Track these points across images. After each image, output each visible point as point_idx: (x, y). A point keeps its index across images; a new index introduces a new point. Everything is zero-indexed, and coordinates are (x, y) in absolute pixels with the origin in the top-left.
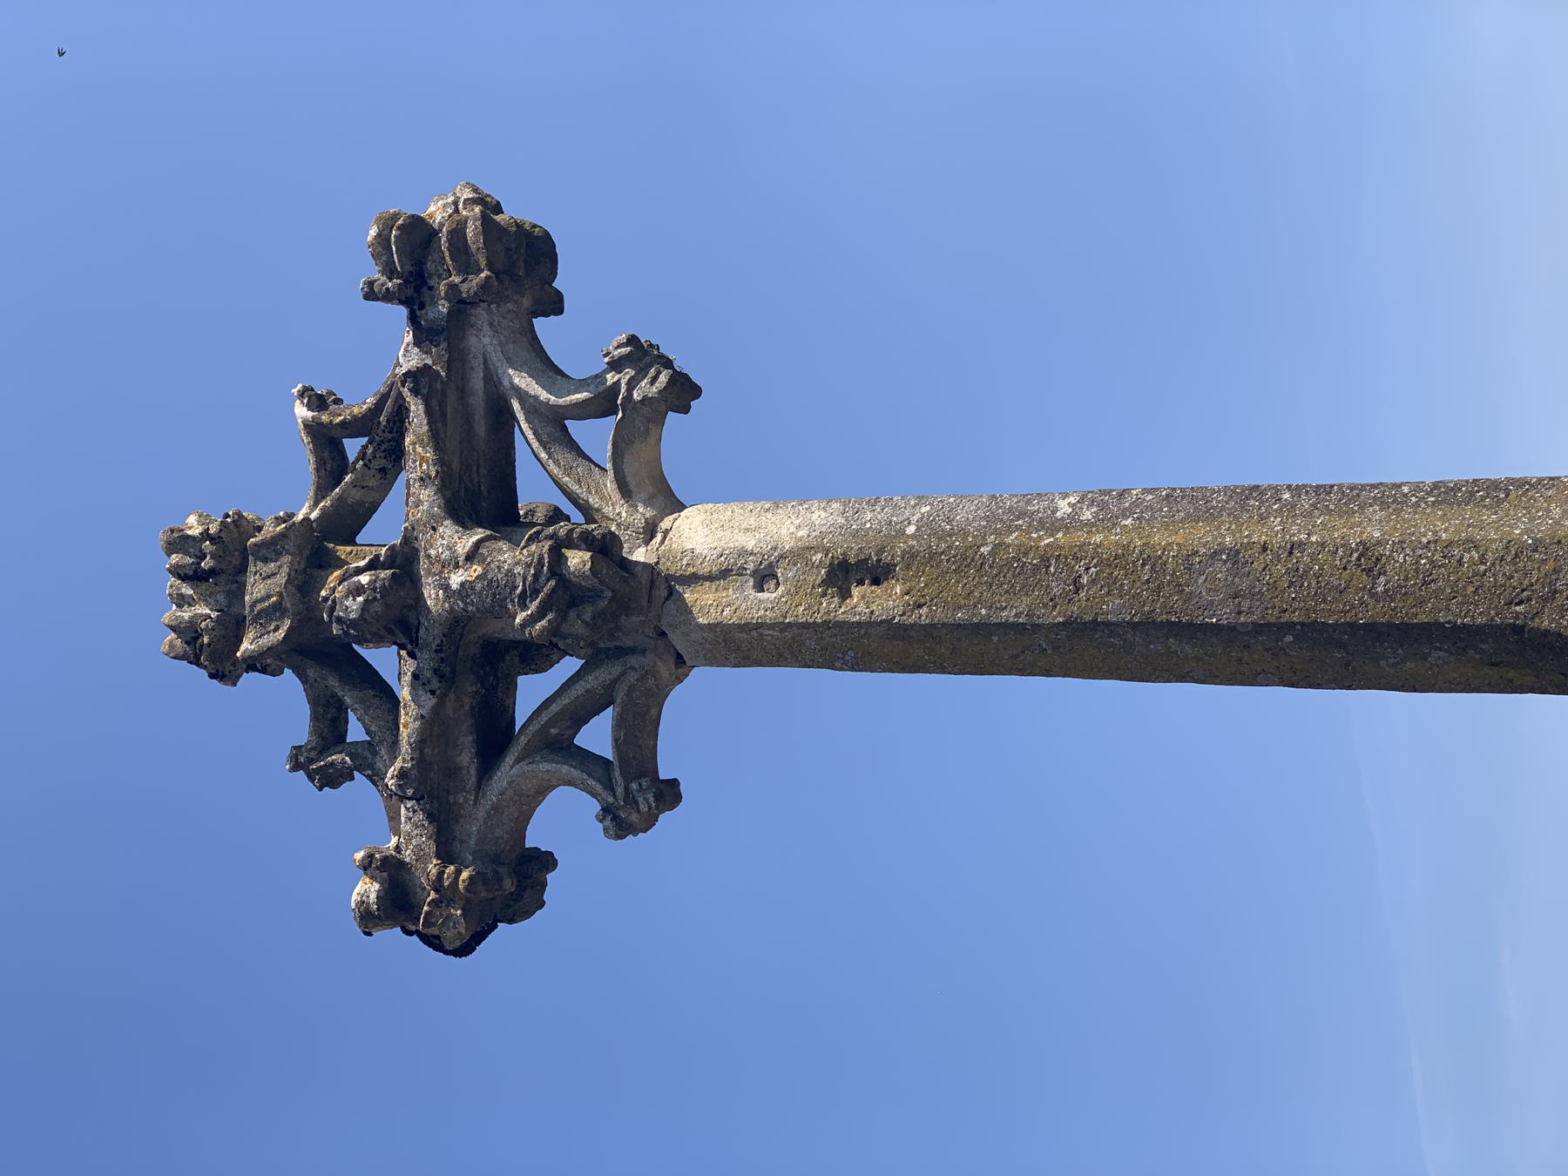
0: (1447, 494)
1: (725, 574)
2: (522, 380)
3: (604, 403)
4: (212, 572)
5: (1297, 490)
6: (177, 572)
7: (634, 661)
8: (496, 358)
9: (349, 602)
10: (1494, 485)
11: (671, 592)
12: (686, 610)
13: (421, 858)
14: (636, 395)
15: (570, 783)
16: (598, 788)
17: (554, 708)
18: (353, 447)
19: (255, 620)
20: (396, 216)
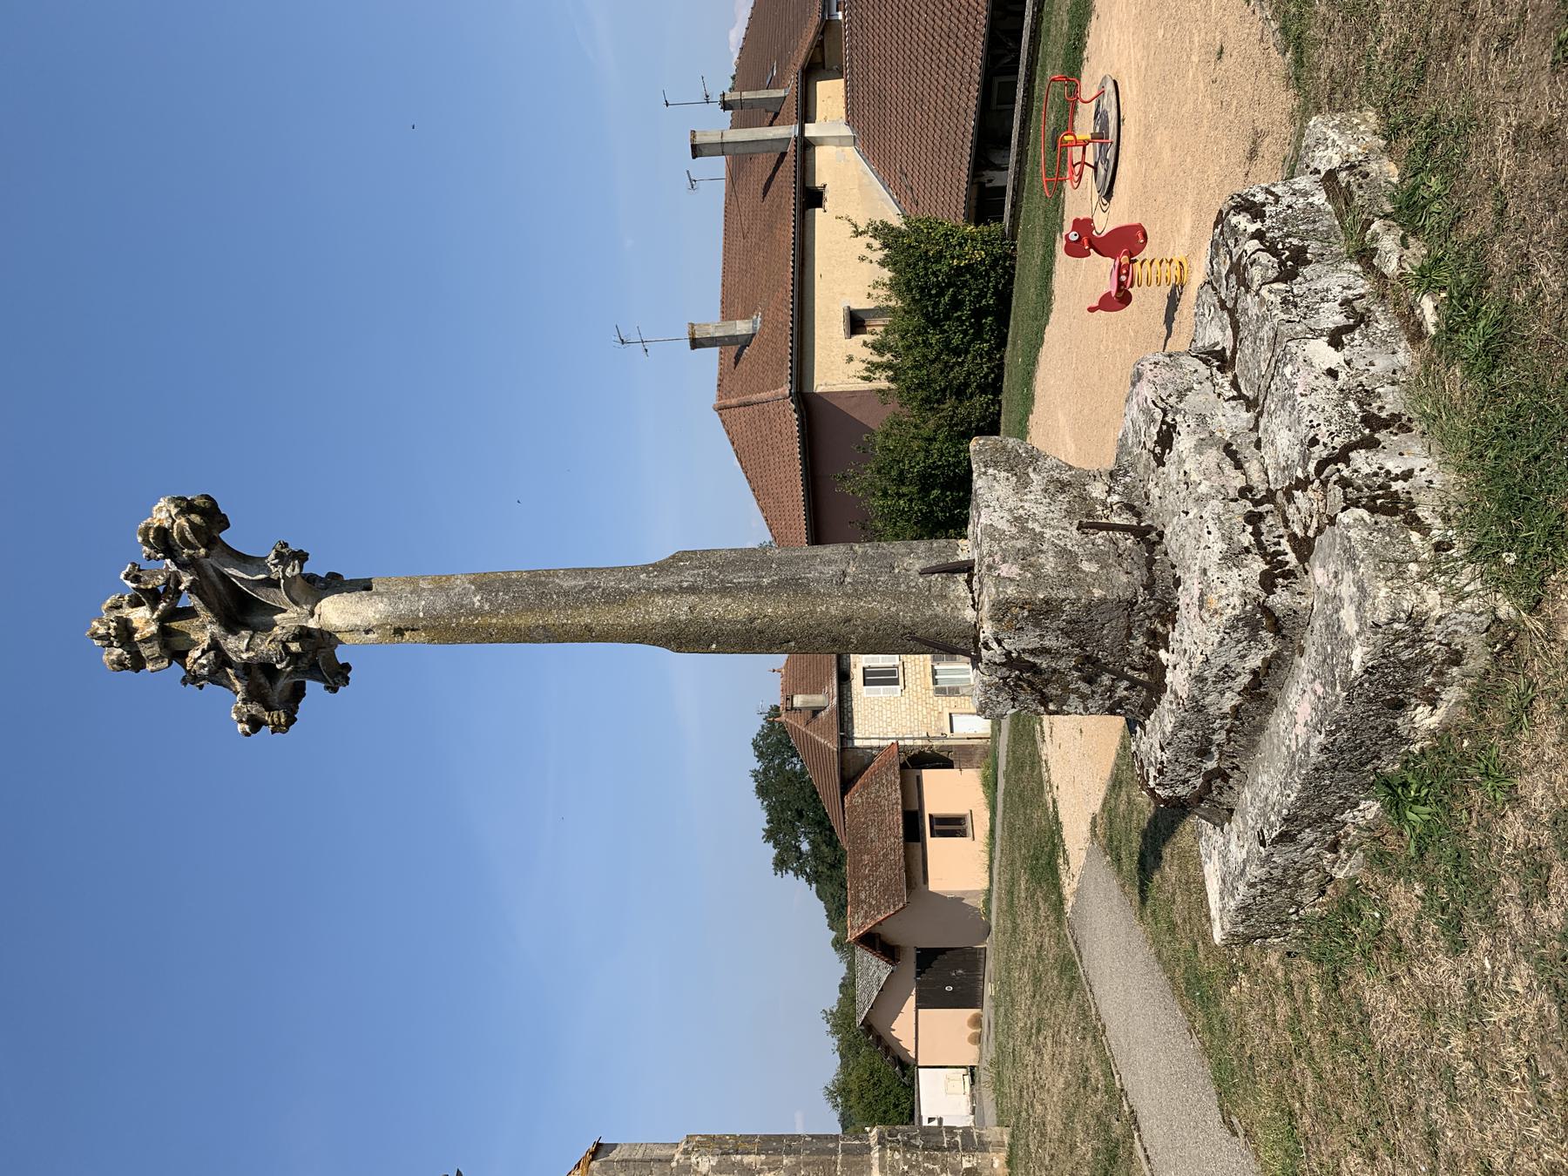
8: (217, 565)
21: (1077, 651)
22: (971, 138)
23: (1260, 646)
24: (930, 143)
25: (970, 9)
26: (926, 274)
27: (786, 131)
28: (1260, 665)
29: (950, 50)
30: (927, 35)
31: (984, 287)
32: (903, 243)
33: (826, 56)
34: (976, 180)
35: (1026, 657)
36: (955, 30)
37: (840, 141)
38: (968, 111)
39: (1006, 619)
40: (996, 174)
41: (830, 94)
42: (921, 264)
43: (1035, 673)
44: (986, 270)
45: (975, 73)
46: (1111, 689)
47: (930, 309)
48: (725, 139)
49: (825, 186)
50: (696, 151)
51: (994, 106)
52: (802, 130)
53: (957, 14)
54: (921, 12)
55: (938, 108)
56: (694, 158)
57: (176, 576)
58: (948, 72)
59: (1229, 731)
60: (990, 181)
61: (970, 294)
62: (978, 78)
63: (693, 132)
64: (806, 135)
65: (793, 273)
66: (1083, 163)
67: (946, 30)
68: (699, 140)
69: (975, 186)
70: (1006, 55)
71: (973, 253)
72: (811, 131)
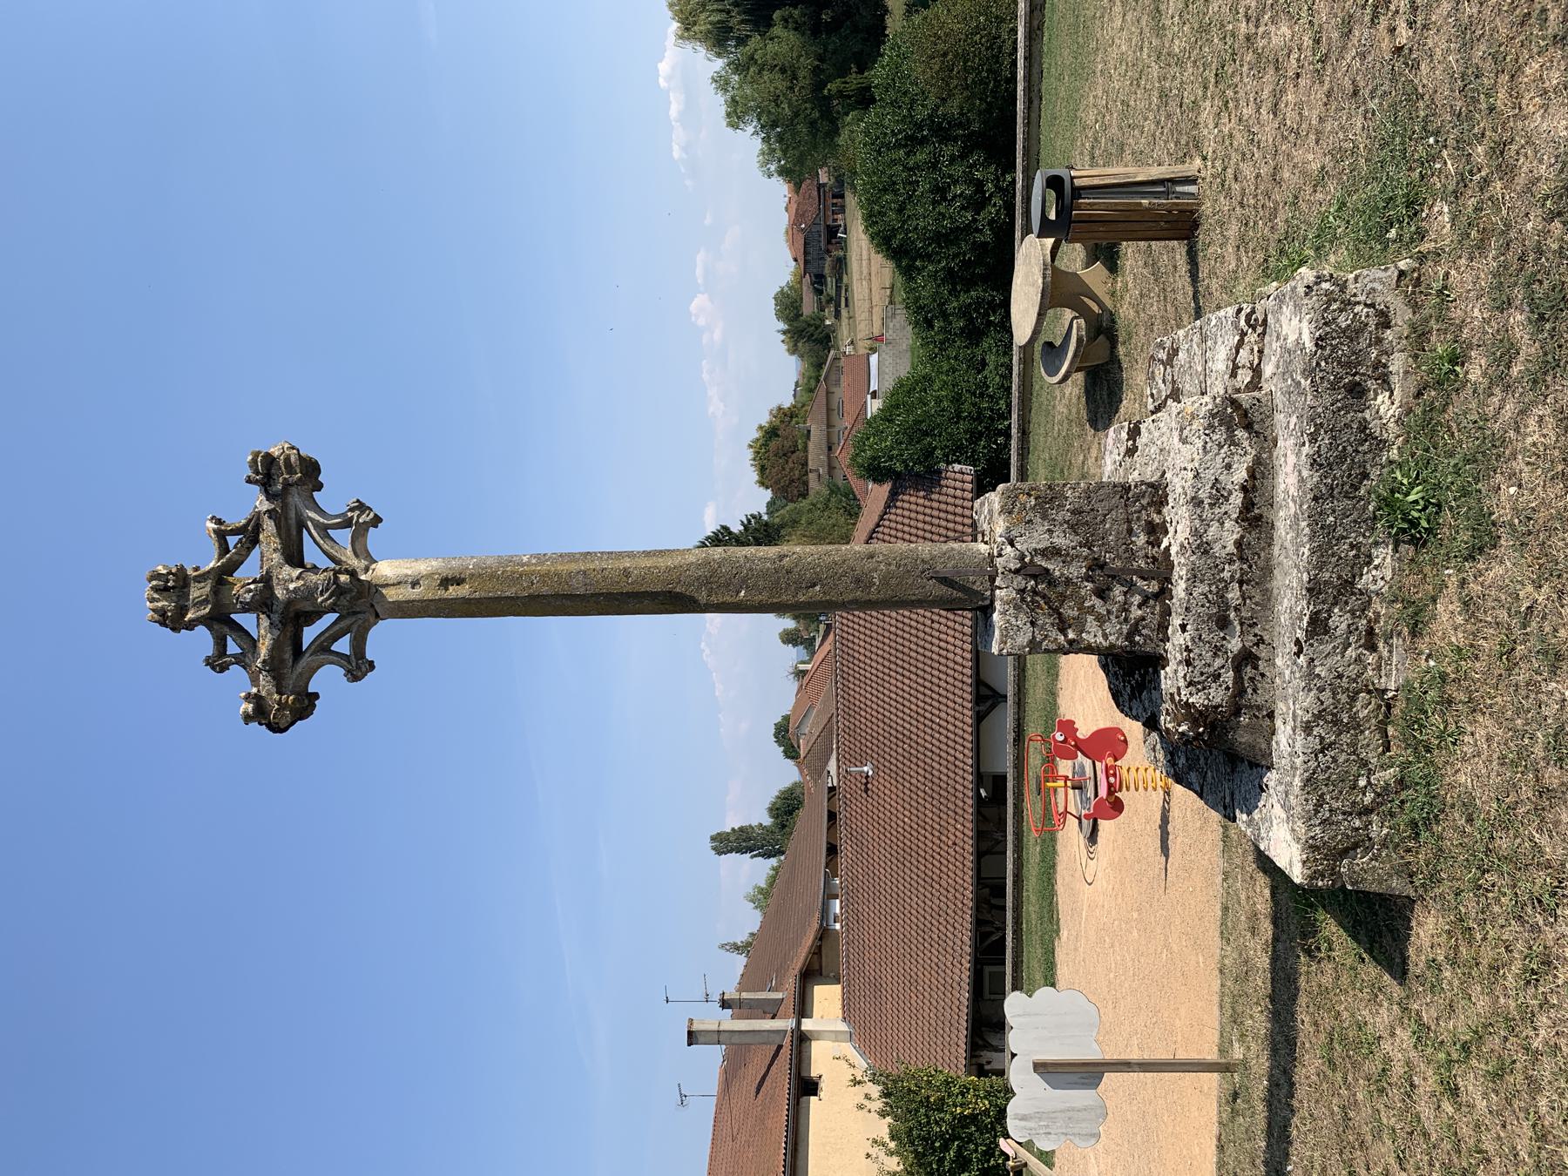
0: (647, 554)
1: (399, 583)
2: (312, 514)
3: (347, 523)
4: (173, 587)
5: (602, 553)
6: (155, 589)
7: (360, 616)
8: (301, 505)
9: (246, 595)
10: (661, 551)
11: (377, 590)
12: (383, 596)
13: (269, 694)
14: (361, 521)
15: (332, 663)
16: (346, 663)
17: (327, 635)
18: (232, 541)
19: (194, 605)
20: (259, 452)
21: (1085, 551)
22: (966, 1011)
23: (1240, 451)
24: (927, 1023)
26: (928, 1123)
27: (785, 1024)
28: (1247, 478)
29: (941, 927)
30: (919, 916)
31: (991, 1142)
32: (903, 1088)
33: (824, 964)
34: (974, 1061)
35: (1039, 560)
36: (945, 908)
37: (836, 1036)
38: (962, 983)
39: (1016, 510)
40: (995, 1055)
41: (827, 998)
42: (922, 1111)
43: (1049, 583)
44: (991, 1123)
46: (1125, 608)
47: (934, 1166)
48: (721, 1028)
49: (820, 1077)
50: (692, 1038)
51: (987, 995)
52: (799, 1023)
53: (945, 893)
54: (913, 896)
55: (932, 986)
56: (689, 1045)
57: (258, 519)
58: (940, 949)
59: (1241, 583)
60: (989, 1063)
61: (976, 1151)
62: (968, 950)
63: (691, 1021)
64: (803, 1028)
65: (785, 1154)
67: (936, 909)
68: (694, 1028)
69: (974, 1067)
70: (993, 933)
71: (976, 1103)
72: (807, 1025)
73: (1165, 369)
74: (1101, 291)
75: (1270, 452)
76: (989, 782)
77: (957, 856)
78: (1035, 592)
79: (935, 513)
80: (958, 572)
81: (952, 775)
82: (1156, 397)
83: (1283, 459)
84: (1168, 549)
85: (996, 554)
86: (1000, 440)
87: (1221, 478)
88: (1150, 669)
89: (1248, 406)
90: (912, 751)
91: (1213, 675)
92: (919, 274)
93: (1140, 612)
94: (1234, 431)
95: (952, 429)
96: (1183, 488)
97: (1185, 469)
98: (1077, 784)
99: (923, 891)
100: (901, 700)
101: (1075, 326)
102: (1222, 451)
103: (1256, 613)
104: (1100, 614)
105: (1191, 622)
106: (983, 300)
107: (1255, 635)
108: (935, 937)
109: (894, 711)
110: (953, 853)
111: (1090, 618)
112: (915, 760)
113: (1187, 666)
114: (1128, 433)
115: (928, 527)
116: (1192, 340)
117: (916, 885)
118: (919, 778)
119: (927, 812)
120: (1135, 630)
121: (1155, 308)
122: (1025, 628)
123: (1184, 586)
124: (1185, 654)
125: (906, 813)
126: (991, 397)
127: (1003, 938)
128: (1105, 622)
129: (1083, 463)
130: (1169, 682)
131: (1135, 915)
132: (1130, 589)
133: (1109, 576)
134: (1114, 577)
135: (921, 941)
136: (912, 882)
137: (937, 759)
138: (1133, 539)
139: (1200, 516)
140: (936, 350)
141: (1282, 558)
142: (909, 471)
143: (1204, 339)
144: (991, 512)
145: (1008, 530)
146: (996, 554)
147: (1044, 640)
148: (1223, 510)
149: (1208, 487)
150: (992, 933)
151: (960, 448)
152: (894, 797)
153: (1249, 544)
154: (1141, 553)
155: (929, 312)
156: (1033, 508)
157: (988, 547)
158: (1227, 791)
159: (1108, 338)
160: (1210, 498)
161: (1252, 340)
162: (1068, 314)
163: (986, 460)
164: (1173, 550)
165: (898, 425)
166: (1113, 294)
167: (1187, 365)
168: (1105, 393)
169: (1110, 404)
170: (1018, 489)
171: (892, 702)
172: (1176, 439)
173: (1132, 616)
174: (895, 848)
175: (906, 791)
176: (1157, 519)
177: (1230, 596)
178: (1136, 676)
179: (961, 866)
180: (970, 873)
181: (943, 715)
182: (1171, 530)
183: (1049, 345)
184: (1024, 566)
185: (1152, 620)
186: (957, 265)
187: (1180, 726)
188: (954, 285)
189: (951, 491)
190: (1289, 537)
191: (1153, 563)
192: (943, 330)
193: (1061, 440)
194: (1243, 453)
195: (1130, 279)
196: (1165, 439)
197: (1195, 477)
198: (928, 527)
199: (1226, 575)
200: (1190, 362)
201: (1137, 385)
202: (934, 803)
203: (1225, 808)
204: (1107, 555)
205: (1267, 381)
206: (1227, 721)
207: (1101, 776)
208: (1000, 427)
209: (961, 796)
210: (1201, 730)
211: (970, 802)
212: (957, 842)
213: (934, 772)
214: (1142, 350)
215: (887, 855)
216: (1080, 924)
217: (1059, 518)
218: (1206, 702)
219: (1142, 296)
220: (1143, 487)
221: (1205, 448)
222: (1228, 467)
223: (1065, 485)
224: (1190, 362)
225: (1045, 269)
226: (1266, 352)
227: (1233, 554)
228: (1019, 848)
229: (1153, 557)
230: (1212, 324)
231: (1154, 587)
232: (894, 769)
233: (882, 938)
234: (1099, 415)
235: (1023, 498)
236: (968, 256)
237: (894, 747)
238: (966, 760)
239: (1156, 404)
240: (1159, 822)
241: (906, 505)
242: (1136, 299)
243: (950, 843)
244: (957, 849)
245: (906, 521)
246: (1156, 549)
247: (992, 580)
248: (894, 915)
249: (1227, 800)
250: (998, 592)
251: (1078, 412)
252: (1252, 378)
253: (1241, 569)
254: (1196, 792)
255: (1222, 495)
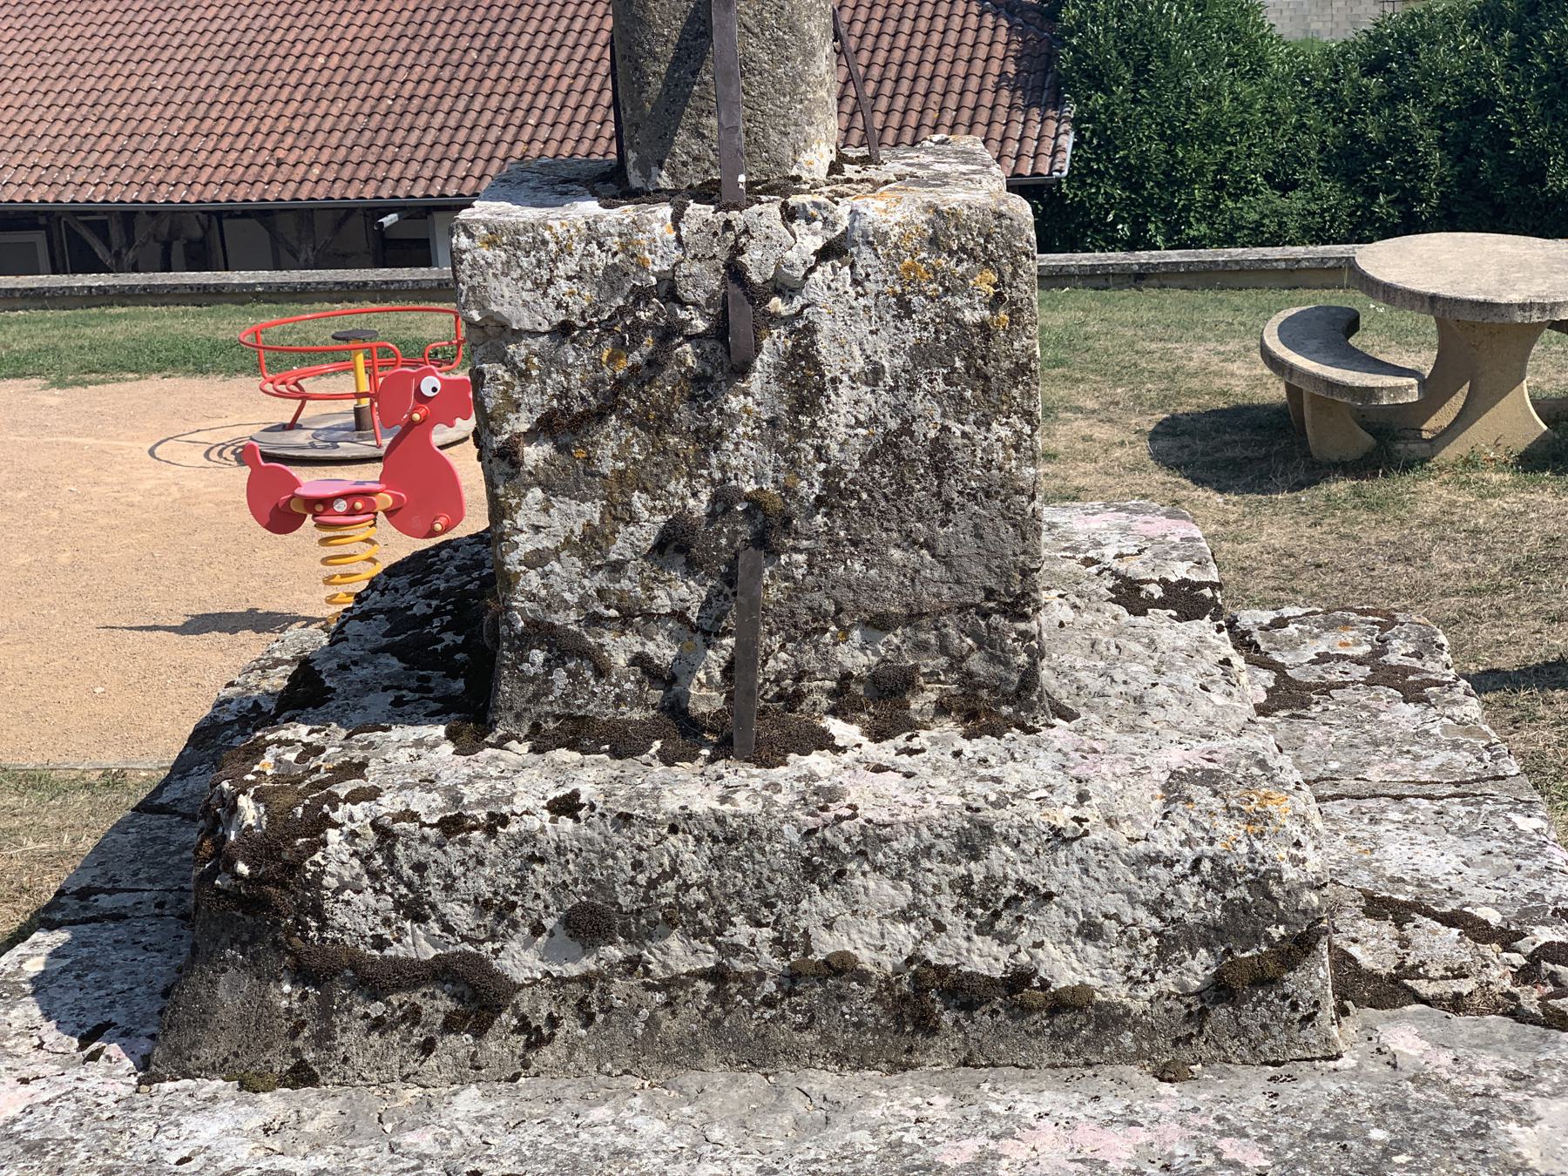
21: (808, 489)
23: (1142, 964)
25: (192, 171)
29: (107, 140)
30: (125, 94)
35: (772, 348)
39: (944, 261)
45: (76, 192)
46: (631, 616)
53: (178, 146)
54: (164, 79)
58: (62, 140)
59: (718, 976)
62: (67, 197)
66: (304, 398)
67: (143, 129)
70: (109, 247)
73: (1359, 661)
74: (1478, 435)
75: (1137, 1057)
76: (413, 231)
77: (254, 169)
78: (669, 333)
79: (970, 99)
80: (728, 74)
81: (420, 154)
82: (1278, 633)
83: (1117, 1108)
84: (825, 742)
85: (794, 200)
86: (1123, 229)
87: (1054, 912)
88: (460, 684)
89: (1289, 987)
90: (465, 69)
91: (418, 900)
92: (1483, 39)
93: (621, 660)
94: (1208, 945)
95: (1149, 127)
96: (1021, 793)
97: (1082, 797)
98: (366, 420)
99: (179, 99)
100: (570, 41)
101: (1403, 381)
102: (1142, 913)
103: (625, 1022)
104: (610, 538)
105: (585, 831)
106: (1422, 179)
107: (553, 1021)
108: (87, 128)
109: (546, 27)
110: (260, 161)
111: (593, 511)
112: (446, 74)
113: (440, 824)
114: (1184, 582)
115: (939, 85)
116: (1456, 746)
117: (188, 84)
118: (409, 86)
119: (340, 104)
120: (562, 647)
121: (1450, 566)
122: (548, 306)
123: (699, 807)
124: (482, 815)
125: (335, 60)
126: (1214, 206)
127: (98, 267)
128: (583, 557)
129: (1079, 409)
130: (403, 757)
131: (64, 559)
132: (695, 629)
133: (732, 564)
134: (730, 579)
135: (76, 101)
136: (193, 77)
137: (452, 123)
138: (856, 634)
139: (928, 851)
140: (1318, 84)
141: (798, 1104)
142: (1060, 39)
143: (1467, 788)
144: (942, 180)
145: (876, 239)
146: (794, 200)
147: (512, 367)
148: (948, 917)
149: (1024, 872)
150: (109, 246)
151: (1108, 145)
152: (367, 31)
153: (841, 998)
154: (810, 658)
155: (1402, 65)
156: (950, 317)
157: (821, 172)
158: (127, 900)
159: (1368, 455)
160: (989, 878)
161: (1494, 973)
162: (1424, 360)
163: (1081, 202)
164: (819, 763)
165: (1159, 9)
166: (1470, 463)
167: (1379, 734)
168: (1237, 452)
169: (1212, 465)
170: (1016, 265)
171: (564, 22)
172: (1175, 757)
173: (608, 638)
174: (261, 39)
175: (380, 57)
176: (919, 704)
177: (675, 943)
178: (449, 637)
179: (235, 177)
180: (223, 197)
181: (544, 132)
182: (884, 751)
183: (1352, 324)
184: (756, 296)
185: (597, 702)
186: (1499, 121)
187: (257, 798)
188: (1458, 115)
189: (1016, 129)
190: (862, 1138)
191: (779, 697)
192: (1361, 93)
193: (1128, 357)
194: (1136, 973)
195: (1511, 502)
196: (1176, 711)
197: (1057, 832)
198: (939, 85)
199: (741, 932)
200: (1389, 741)
201: (1260, 527)
202: (361, 118)
203: (84, 894)
204: (801, 558)
205: (1369, 1035)
206: (276, 943)
207: (349, 477)
208: (1151, 227)
209: (380, 174)
210: (243, 868)
211: (368, 193)
212: (284, 168)
213: (424, 117)
214: (1342, 537)
215: (245, 21)
216: (70, 433)
217: (919, 403)
218: (329, 881)
219: (1475, 532)
220: (1023, 658)
221: (1153, 859)
222: (1090, 931)
223: (1028, 416)
224: (1389, 741)
225: (1542, 308)
226: (1459, 1020)
227: (808, 950)
228: (275, 295)
229: (798, 696)
230: (1518, 820)
231: (704, 699)
232: (425, 32)
233: (75, 18)
234: (1186, 440)
235: (984, 283)
236: (1518, 142)
237: (470, 30)
238: (454, 181)
239: (1257, 636)
240: (264, 608)
241: (985, 36)
242: (1464, 519)
243: (280, 154)
244: (270, 169)
245: (952, 38)
246: (825, 703)
247: (707, 193)
248: (123, 40)
249: (105, 901)
250: (665, 211)
251: (1192, 393)
252: (1372, 976)
253: (761, 976)
254: (159, 789)
255: (996, 915)
